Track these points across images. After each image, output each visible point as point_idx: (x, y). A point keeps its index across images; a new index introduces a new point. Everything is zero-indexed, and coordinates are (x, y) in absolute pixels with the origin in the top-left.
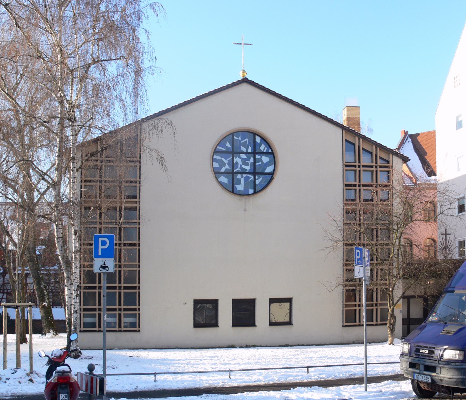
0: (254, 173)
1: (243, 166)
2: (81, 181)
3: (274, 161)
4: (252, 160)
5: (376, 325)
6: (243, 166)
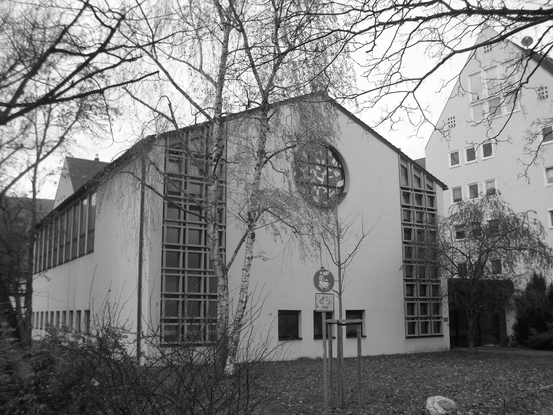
0: (328, 187)
1: (318, 178)
2: (161, 320)
3: (343, 176)
4: (325, 173)
5: (418, 337)
6: (318, 178)
